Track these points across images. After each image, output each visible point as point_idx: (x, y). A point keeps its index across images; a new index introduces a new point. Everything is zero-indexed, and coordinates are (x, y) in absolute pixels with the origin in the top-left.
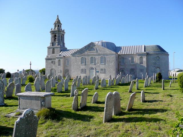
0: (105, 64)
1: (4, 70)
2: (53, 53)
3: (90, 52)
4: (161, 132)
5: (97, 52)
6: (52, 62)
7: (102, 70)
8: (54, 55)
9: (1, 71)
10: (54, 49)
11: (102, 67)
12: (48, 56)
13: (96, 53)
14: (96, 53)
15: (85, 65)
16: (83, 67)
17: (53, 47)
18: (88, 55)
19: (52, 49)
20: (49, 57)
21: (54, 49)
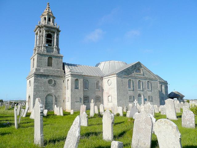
0: (151, 91)
1: (183, 96)
2: (50, 64)
3: (137, 73)
4: (36, 116)
5: (144, 75)
6: (50, 82)
7: (149, 97)
8: (50, 68)
9: (1, 101)
10: (50, 58)
11: (149, 93)
12: (39, 70)
13: (142, 76)
14: (142, 76)
15: (133, 90)
16: (131, 93)
17: (49, 54)
18: (136, 78)
19: (47, 58)
20: (42, 71)
21: (50, 58)
